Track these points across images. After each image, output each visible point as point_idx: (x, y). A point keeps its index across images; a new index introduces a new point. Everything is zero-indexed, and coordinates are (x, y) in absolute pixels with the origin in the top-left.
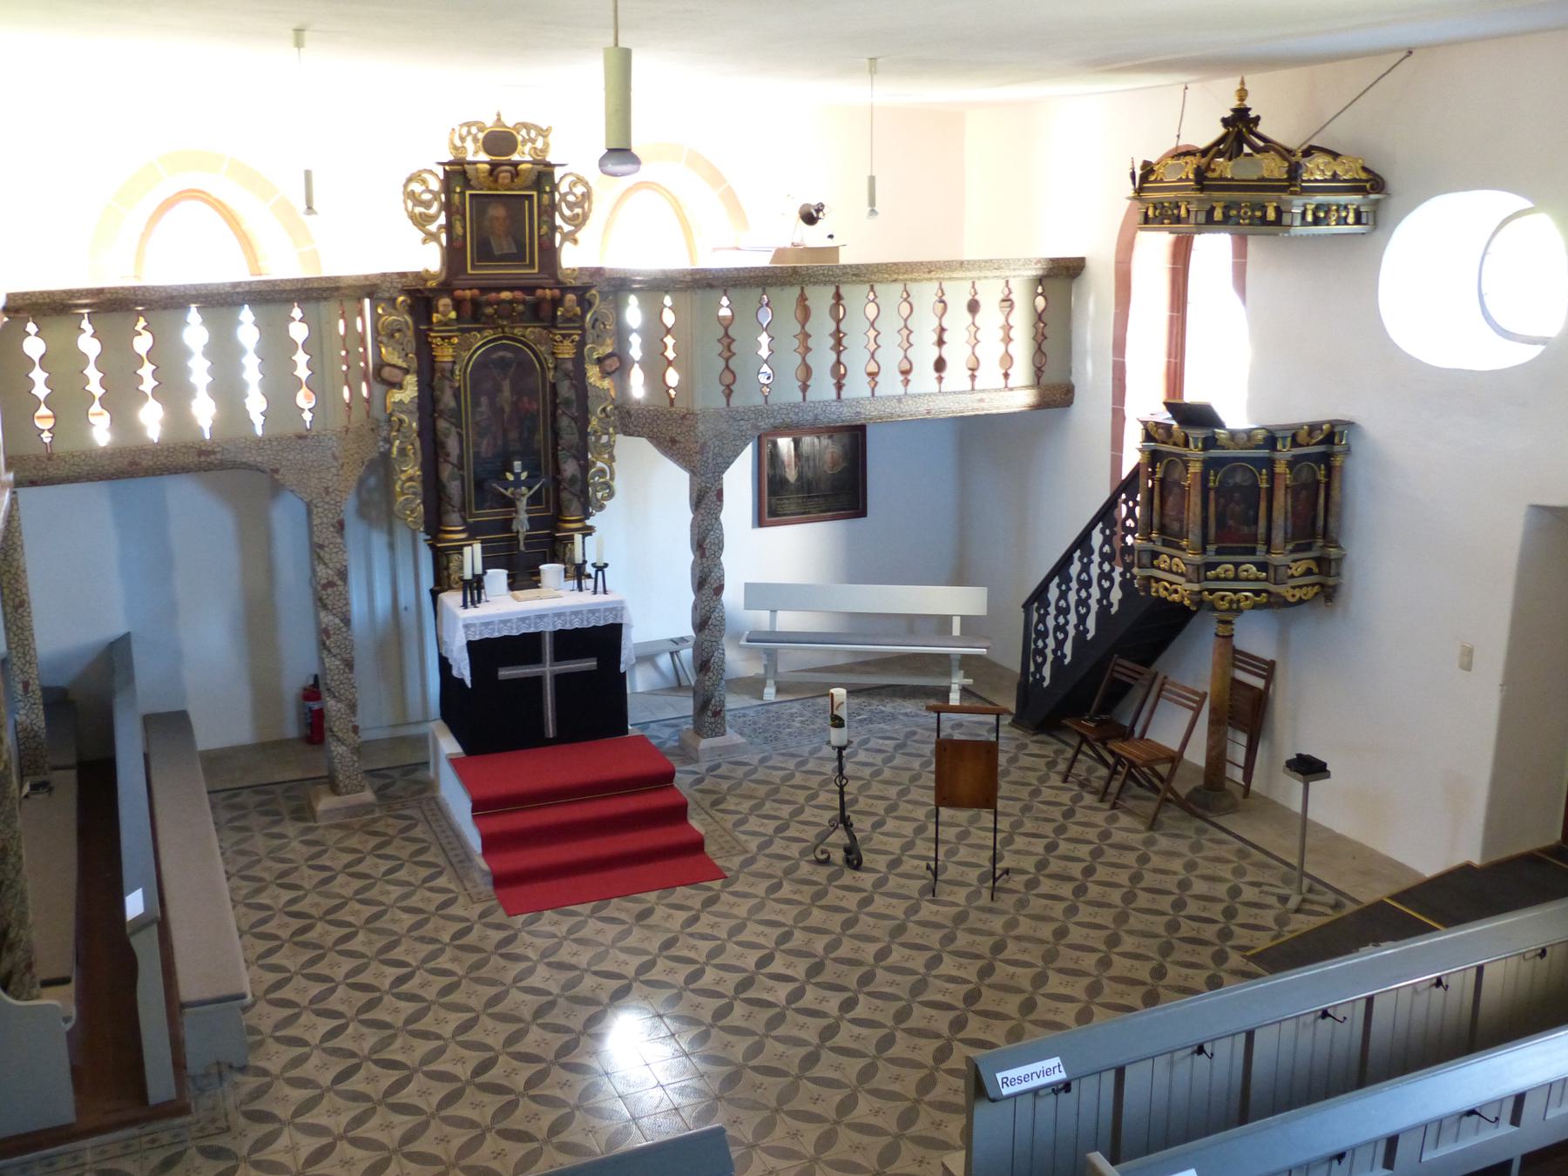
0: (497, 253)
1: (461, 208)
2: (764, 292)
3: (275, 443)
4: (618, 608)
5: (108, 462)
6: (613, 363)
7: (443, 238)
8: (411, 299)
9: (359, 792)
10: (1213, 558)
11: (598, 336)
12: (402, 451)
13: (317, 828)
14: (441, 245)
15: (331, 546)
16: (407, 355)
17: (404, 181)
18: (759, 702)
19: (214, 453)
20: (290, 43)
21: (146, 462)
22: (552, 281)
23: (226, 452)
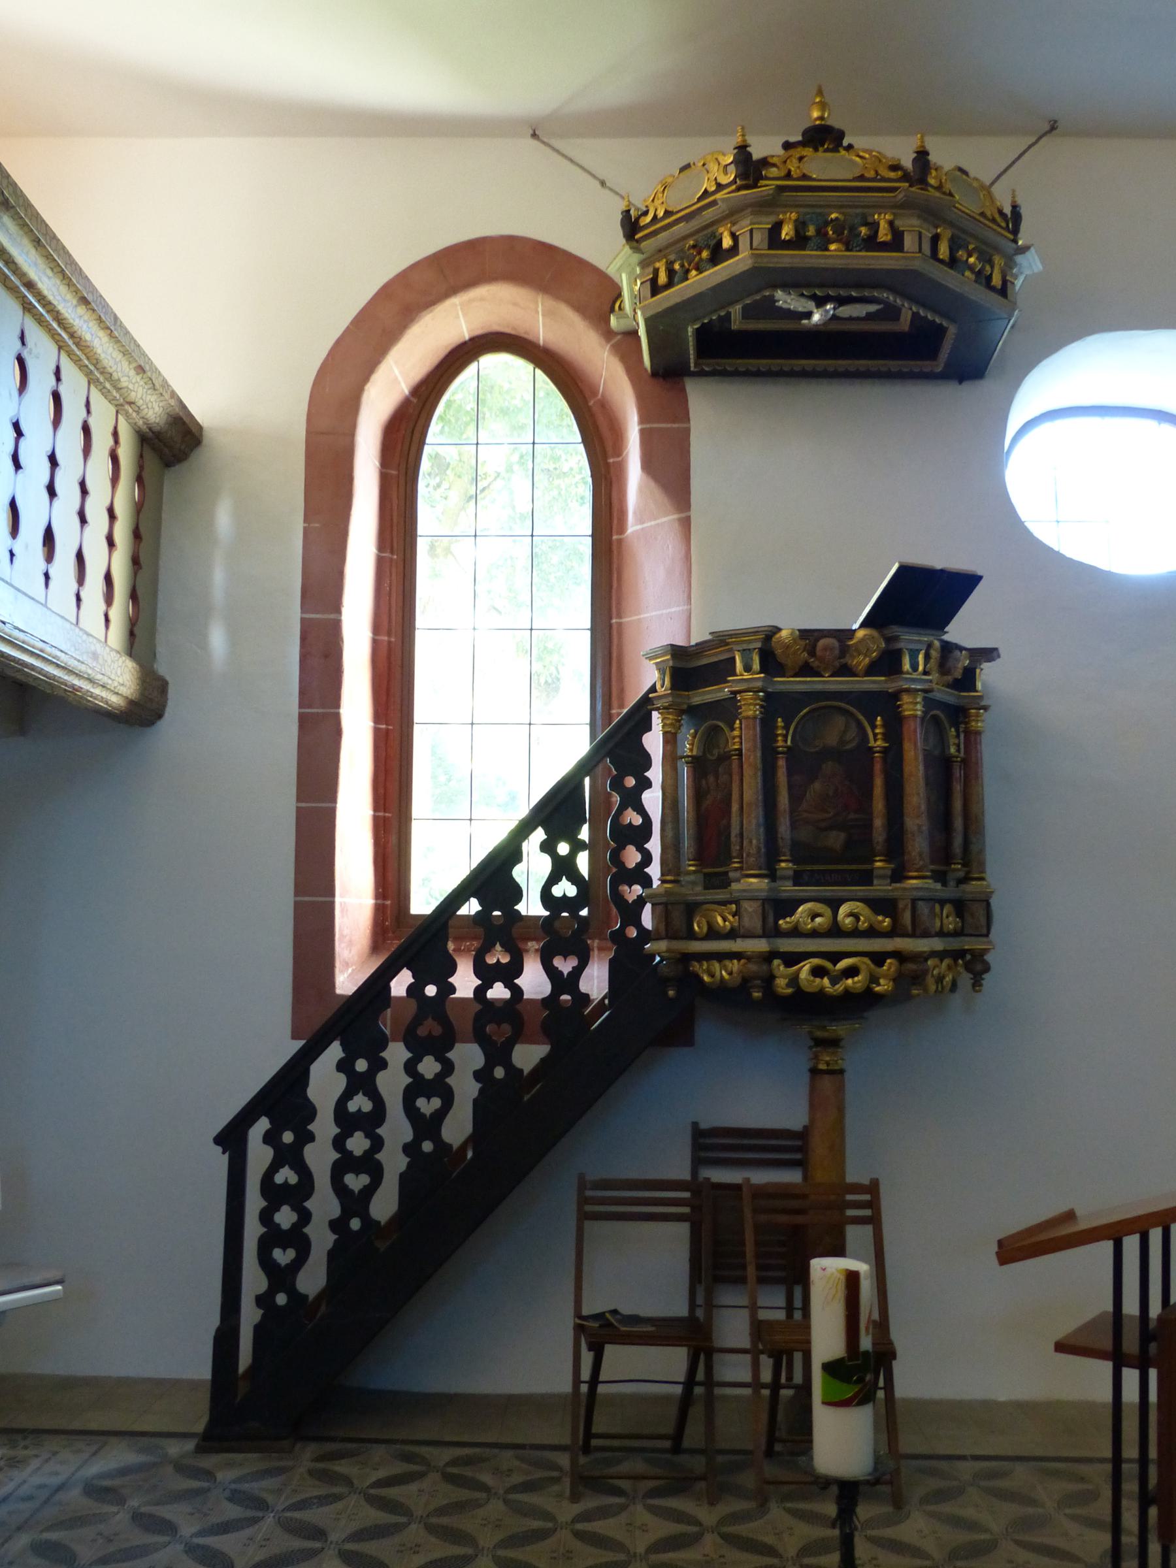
10: (788, 889)
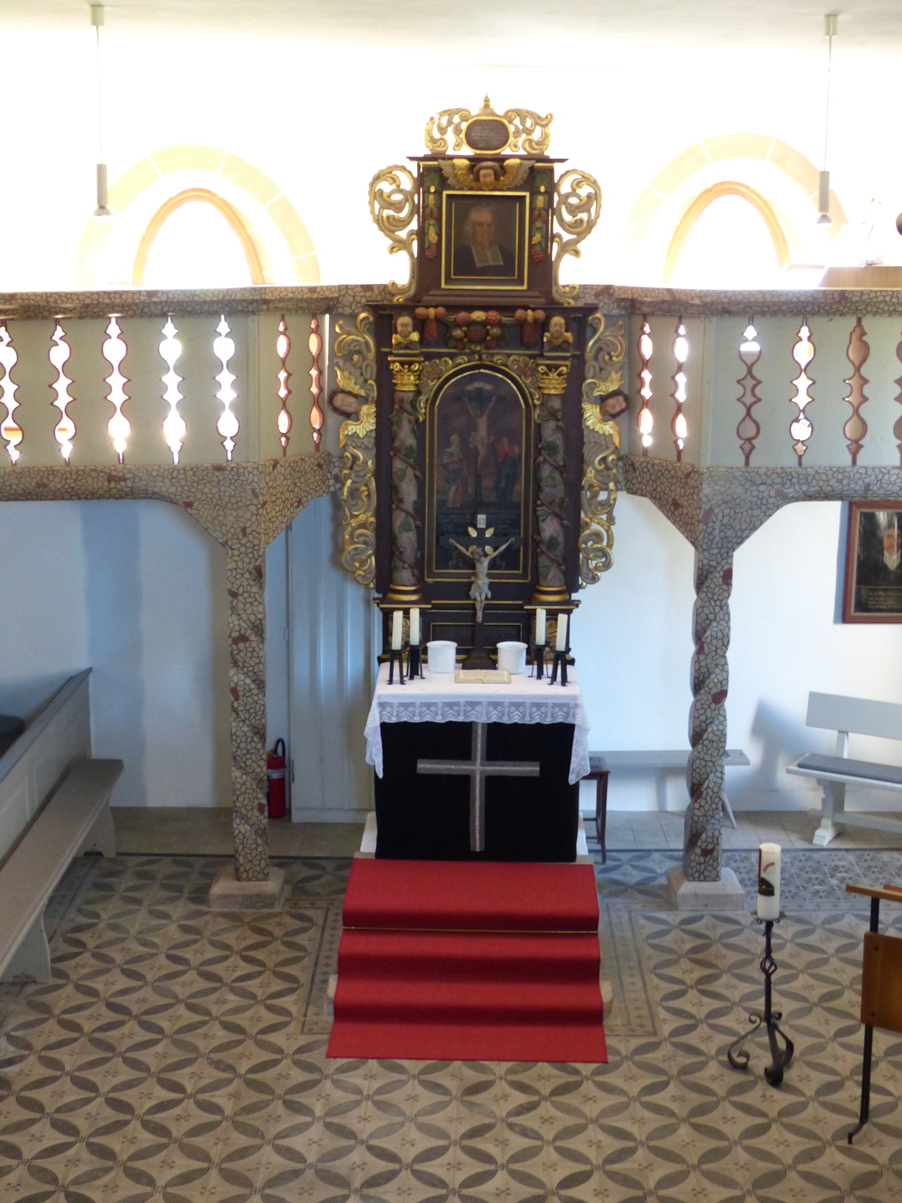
0: (479, 265)
1: (435, 211)
4: (570, 706)
5: (16, 482)
6: (618, 404)
7: (415, 245)
8: (373, 316)
9: (262, 880)
11: (601, 369)
12: (353, 493)
13: (205, 914)
14: (411, 255)
15: (246, 595)
16: (366, 381)
17: (370, 180)
18: (806, 845)
19: (125, 480)
20: (88, 19)
21: (55, 484)
22: (543, 300)
23: (137, 480)
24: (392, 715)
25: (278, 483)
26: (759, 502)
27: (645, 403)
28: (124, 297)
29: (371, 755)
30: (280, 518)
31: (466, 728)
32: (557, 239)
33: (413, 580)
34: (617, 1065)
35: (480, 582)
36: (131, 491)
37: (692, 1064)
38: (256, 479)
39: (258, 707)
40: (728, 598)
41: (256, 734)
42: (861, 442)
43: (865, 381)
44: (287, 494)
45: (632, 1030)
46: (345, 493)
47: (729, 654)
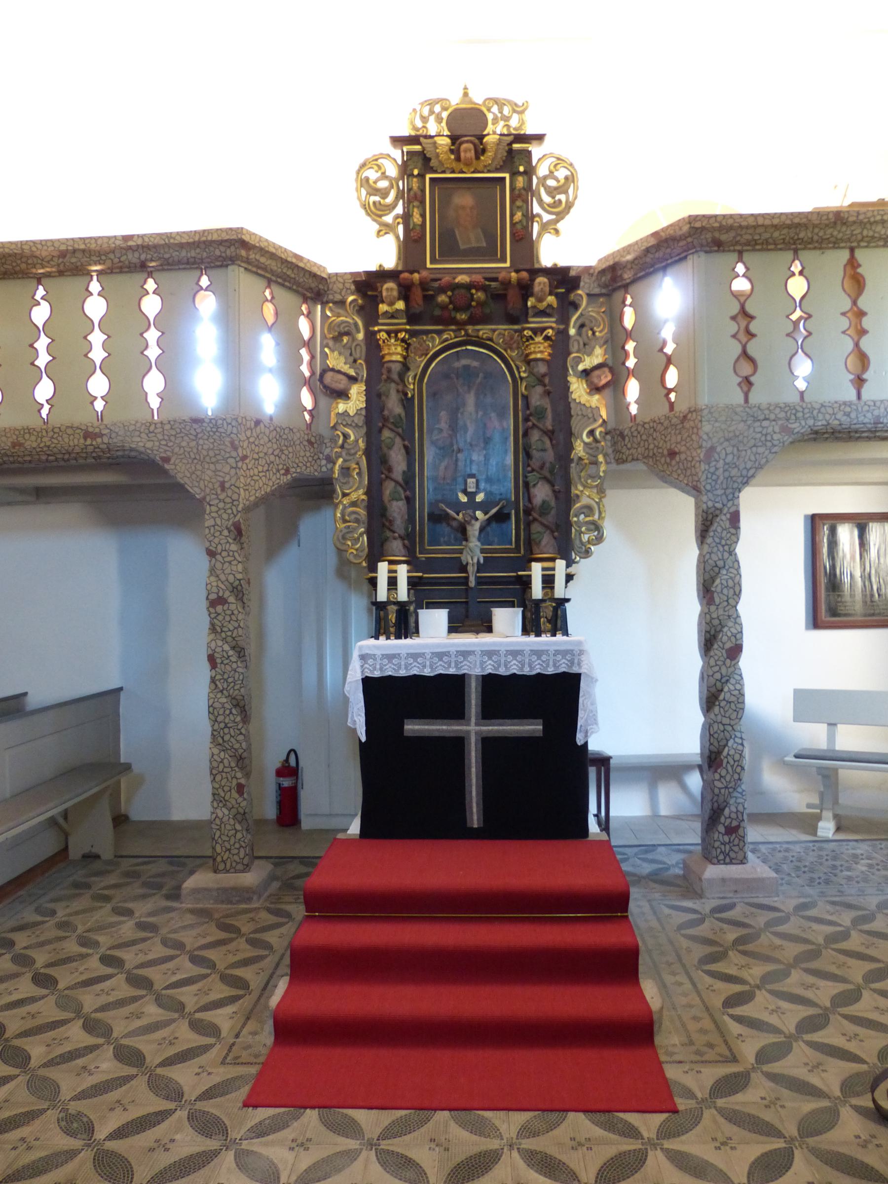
2: (796, 257)
3: (167, 427)
9: (243, 871)
11: (585, 345)
12: (346, 471)
14: (398, 237)
15: (224, 554)
16: (355, 361)
17: (357, 167)
19: (101, 435)
23: (113, 435)
24: (375, 669)
25: (262, 442)
26: (763, 438)
27: (630, 373)
28: (99, 242)
29: (353, 716)
30: (264, 478)
31: (457, 682)
32: (537, 219)
33: (403, 551)
34: (696, 1119)
35: (471, 545)
36: (108, 448)
37: (813, 1112)
38: (235, 431)
39: (237, 675)
40: (737, 542)
41: (235, 706)
42: (865, 376)
43: (861, 314)
44: (272, 458)
45: (698, 1053)
46: (337, 472)
47: (743, 608)
